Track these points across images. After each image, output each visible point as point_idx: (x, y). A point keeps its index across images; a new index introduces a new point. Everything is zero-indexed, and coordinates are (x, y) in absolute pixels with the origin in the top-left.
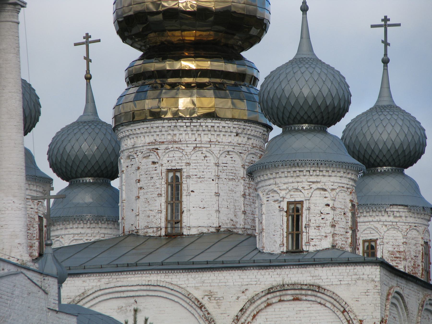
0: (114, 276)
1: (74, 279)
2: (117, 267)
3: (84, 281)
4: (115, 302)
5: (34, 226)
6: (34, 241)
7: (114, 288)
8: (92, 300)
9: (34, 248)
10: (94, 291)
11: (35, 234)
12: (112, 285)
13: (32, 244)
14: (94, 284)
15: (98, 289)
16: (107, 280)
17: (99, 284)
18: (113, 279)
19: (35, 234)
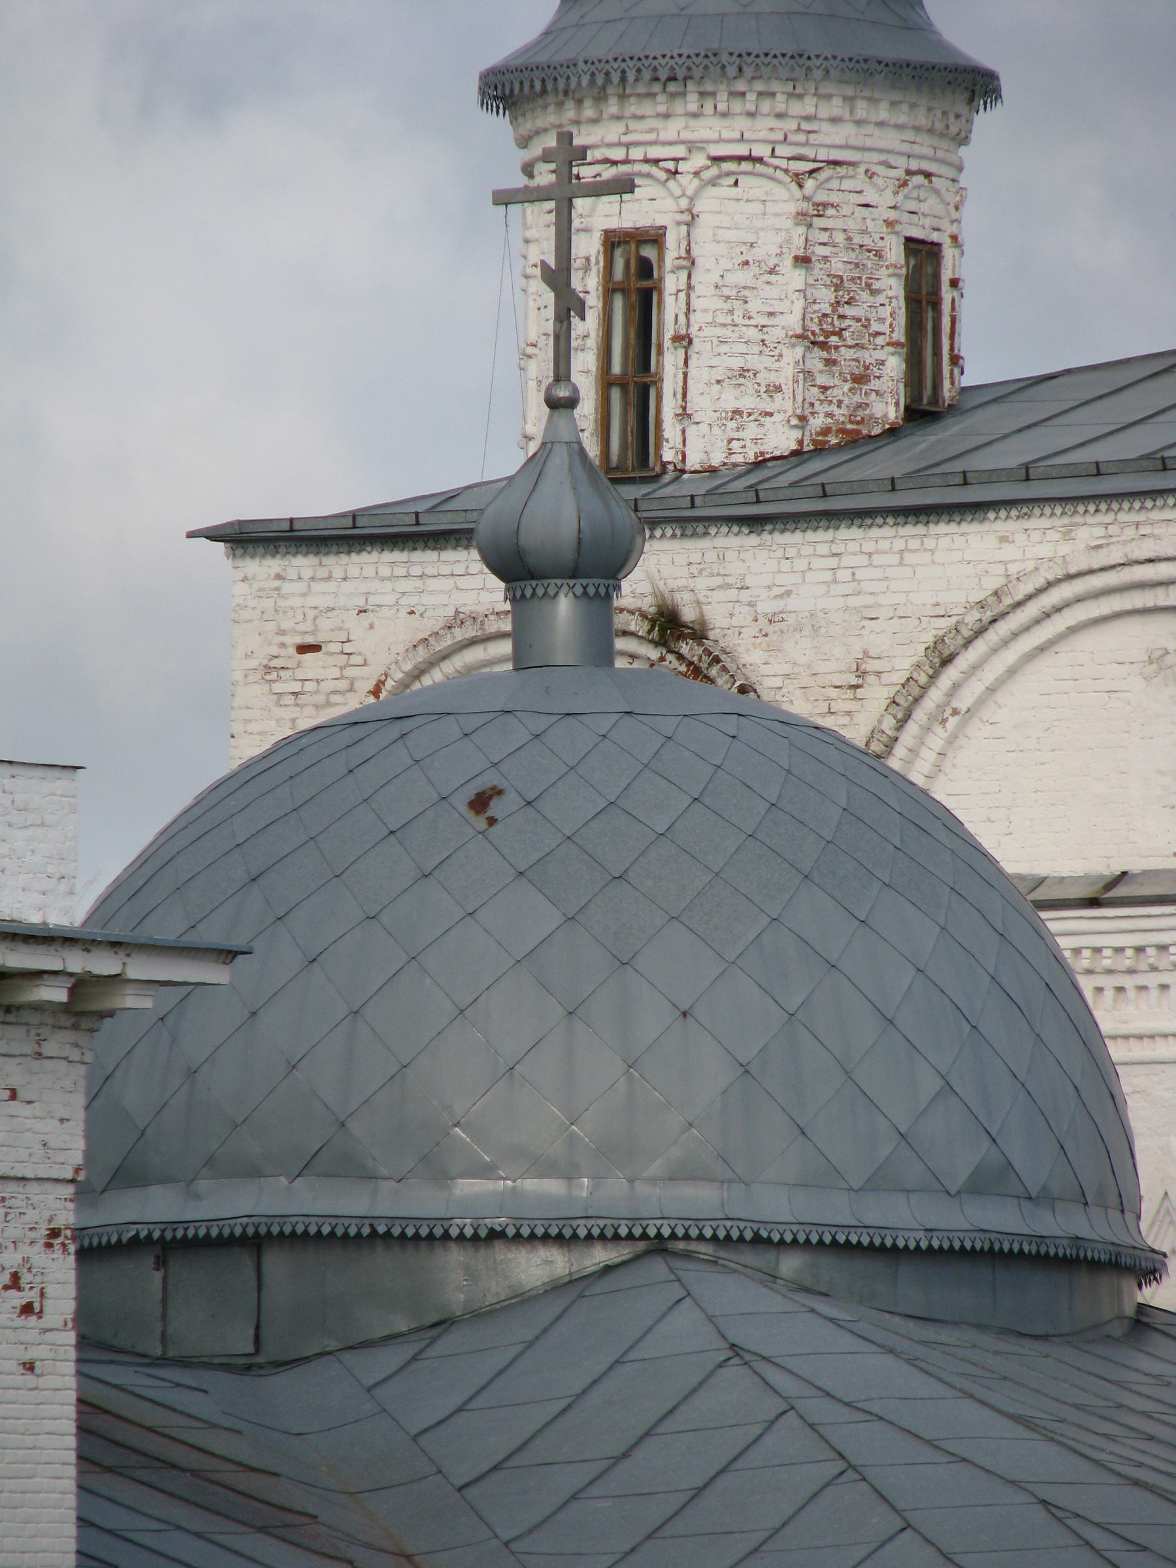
0: (1128, 515)
1: (965, 527)
2: (1165, 469)
3: (1003, 539)
4: (1134, 626)
5: (876, 285)
6: (880, 355)
7: (1127, 569)
8: (1037, 622)
9: (875, 384)
10: (1040, 582)
11: (881, 320)
12: (1116, 556)
13: (867, 368)
14: (1045, 551)
15: (1060, 573)
16: (1100, 531)
17: (1065, 549)
18: (1124, 525)
19: (881, 320)
